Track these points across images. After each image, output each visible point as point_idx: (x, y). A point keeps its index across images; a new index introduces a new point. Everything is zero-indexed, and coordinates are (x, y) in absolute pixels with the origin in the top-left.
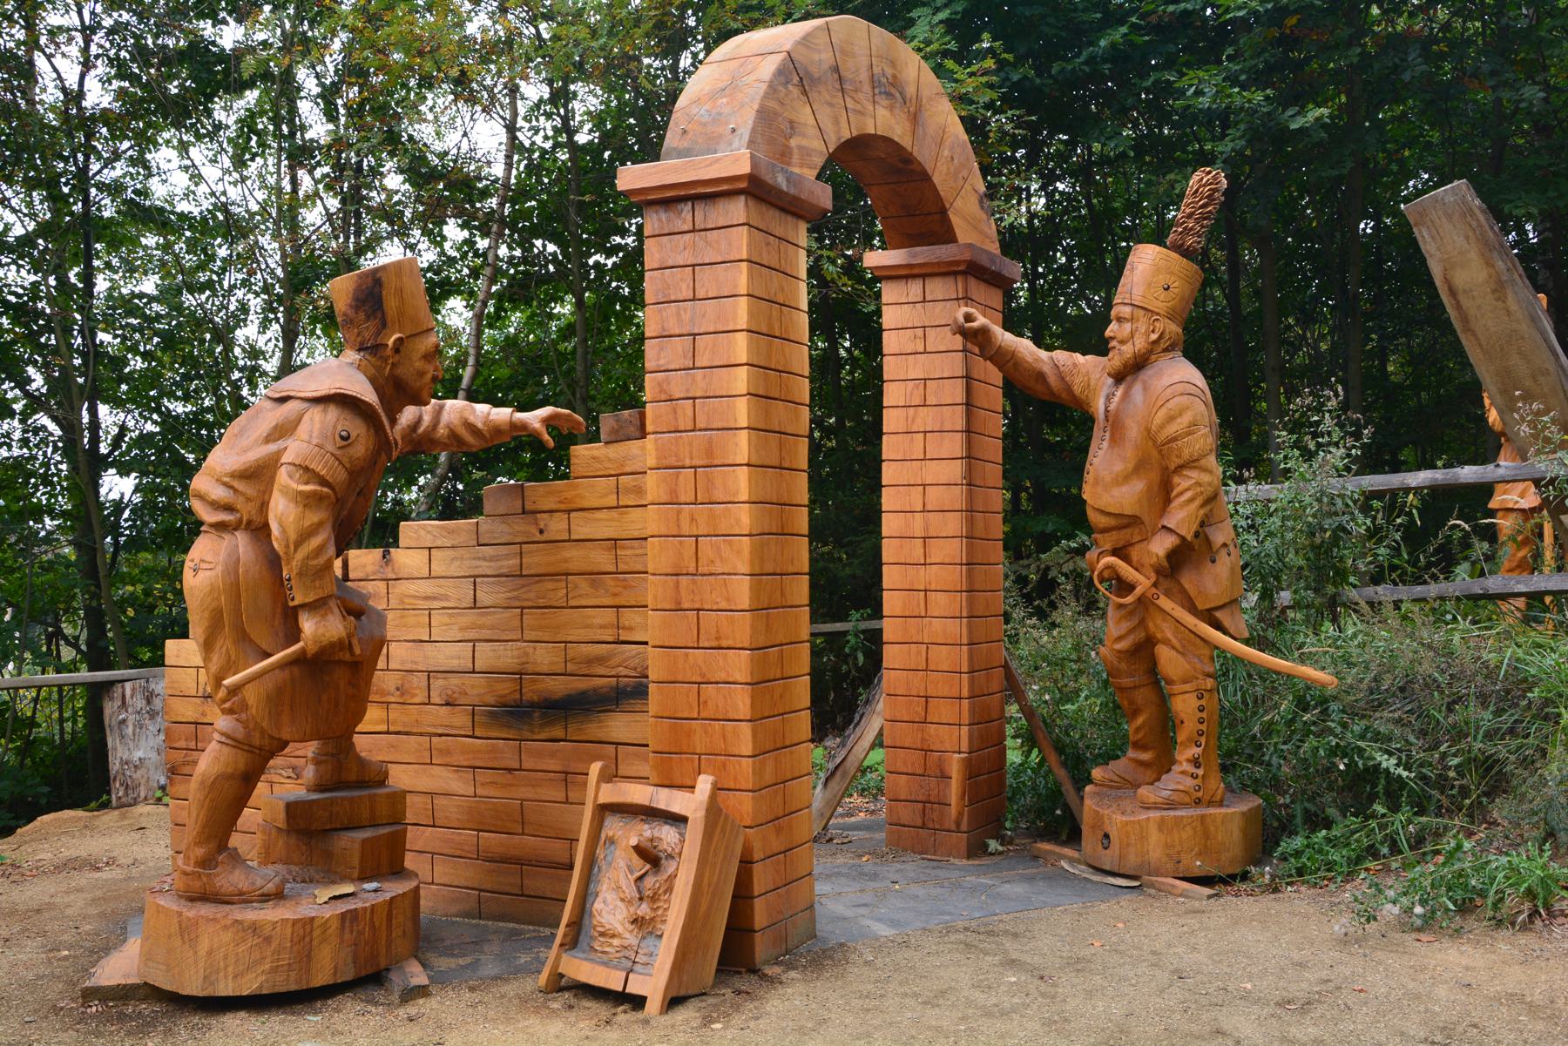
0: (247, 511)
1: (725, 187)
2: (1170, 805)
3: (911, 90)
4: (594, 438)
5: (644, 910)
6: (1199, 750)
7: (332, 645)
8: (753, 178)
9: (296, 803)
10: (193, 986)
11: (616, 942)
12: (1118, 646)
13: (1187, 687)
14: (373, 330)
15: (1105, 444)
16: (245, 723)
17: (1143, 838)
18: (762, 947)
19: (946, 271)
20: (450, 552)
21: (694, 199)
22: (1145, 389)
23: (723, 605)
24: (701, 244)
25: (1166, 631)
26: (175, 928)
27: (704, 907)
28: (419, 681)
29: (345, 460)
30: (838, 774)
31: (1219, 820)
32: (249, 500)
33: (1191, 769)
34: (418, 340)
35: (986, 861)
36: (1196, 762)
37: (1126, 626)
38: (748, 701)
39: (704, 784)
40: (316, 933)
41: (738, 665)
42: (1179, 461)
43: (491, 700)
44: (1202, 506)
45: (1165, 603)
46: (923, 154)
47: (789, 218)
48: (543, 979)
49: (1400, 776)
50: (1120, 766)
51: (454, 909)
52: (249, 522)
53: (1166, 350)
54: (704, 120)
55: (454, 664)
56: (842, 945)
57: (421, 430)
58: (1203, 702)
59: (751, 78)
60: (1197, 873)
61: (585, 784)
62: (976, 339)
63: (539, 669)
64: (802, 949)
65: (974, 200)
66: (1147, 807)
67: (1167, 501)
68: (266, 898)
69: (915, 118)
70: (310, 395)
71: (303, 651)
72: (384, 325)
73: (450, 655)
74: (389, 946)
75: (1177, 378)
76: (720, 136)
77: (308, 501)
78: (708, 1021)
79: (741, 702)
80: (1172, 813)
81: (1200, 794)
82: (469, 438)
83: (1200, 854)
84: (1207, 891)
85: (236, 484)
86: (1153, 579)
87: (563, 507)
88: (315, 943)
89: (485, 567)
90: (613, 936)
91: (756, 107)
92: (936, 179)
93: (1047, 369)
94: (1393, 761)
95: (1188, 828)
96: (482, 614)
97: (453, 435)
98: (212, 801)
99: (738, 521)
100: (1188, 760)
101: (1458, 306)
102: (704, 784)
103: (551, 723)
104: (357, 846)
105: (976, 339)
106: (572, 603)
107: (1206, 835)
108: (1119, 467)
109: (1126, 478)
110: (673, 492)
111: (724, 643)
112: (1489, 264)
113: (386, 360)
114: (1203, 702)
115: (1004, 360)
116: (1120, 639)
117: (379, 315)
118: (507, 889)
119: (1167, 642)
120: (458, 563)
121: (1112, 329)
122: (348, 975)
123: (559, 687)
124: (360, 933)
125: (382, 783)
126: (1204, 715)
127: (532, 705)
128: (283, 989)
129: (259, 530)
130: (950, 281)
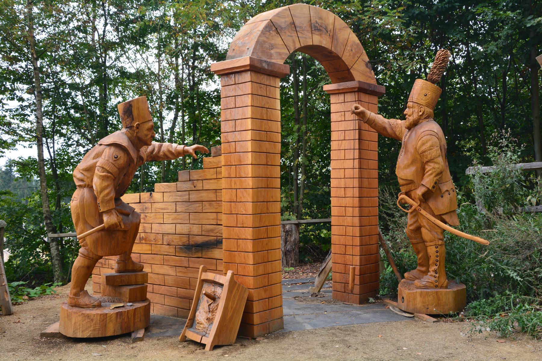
0: (87, 181)
1: (243, 69)
2: (426, 287)
3: (331, 27)
4: (209, 155)
5: (210, 315)
6: (436, 267)
7: (113, 225)
8: (250, 65)
9: (109, 276)
10: (70, 335)
11: (202, 326)
12: (411, 228)
13: (432, 244)
14: (129, 121)
15: (403, 153)
16: (87, 250)
17: (415, 299)
18: (256, 330)
19: (351, 91)
20: (169, 194)
22: (416, 133)
23: (244, 213)
24: (237, 89)
25: (424, 223)
26: (66, 315)
27: (230, 314)
28: (160, 236)
29: (116, 165)
30: (323, 272)
32: (88, 178)
33: (434, 274)
34: (145, 124)
35: (370, 305)
36: (435, 271)
37: (413, 220)
38: (252, 246)
39: (229, 273)
40: (108, 319)
41: (248, 233)
42: (427, 160)
44: (436, 176)
45: (423, 212)
46: (338, 50)
47: (271, 78)
48: (180, 338)
49: (517, 280)
50: (414, 272)
51: (171, 314)
52: (88, 185)
53: (425, 118)
54: (240, 45)
55: (170, 231)
56: (290, 331)
57: (154, 153)
58: (438, 249)
59: (257, 29)
60: (435, 313)
61: (198, 271)
62: (361, 115)
63: (194, 234)
64: (276, 333)
65: (363, 64)
67: (424, 175)
68: (94, 307)
69: (333, 37)
70: (108, 143)
71: (104, 227)
72: (133, 119)
73: (169, 228)
74: (134, 324)
75: (427, 129)
76: (244, 51)
77: (103, 178)
78: (225, 353)
79: (249, 246)
80: (425, 290)
81: (437, 284)
83: (436, 306)
84: (435, 320)
85: (84, 173)
86: (419, 203)
87: (200, 178)
88: (108, 321)
89: (179, 199)
90: (201, 324)
91: (256, 40)
92: (343, 58)
93: (387, 126)
94: (515, 274)
95: (431, 296)
96: (178, 215)
98: (78, 275)
99: (248, 184)
100: (433, 271)
103: (197, 252)
104: (128, 291)
105: (361, 115)
106: (204, 211)
107: (439, 299)
108: (406, 162)
109: (408, 166)
110: (229, 174)
111: (245, 226)
113: (134, 131)
114: (438, 249)
115: (371, 123)
116: (411, 225)
117: (131, 116)
118: (185, 308)
119: (424, 227)
120: (171, 197)
121: (407, 111)
122: (119, 333)
123: (200, 240)
125: (141, 270)
126: (438, 254)
127: (192, 246)
128: (97, 336)
129: (90, 187)
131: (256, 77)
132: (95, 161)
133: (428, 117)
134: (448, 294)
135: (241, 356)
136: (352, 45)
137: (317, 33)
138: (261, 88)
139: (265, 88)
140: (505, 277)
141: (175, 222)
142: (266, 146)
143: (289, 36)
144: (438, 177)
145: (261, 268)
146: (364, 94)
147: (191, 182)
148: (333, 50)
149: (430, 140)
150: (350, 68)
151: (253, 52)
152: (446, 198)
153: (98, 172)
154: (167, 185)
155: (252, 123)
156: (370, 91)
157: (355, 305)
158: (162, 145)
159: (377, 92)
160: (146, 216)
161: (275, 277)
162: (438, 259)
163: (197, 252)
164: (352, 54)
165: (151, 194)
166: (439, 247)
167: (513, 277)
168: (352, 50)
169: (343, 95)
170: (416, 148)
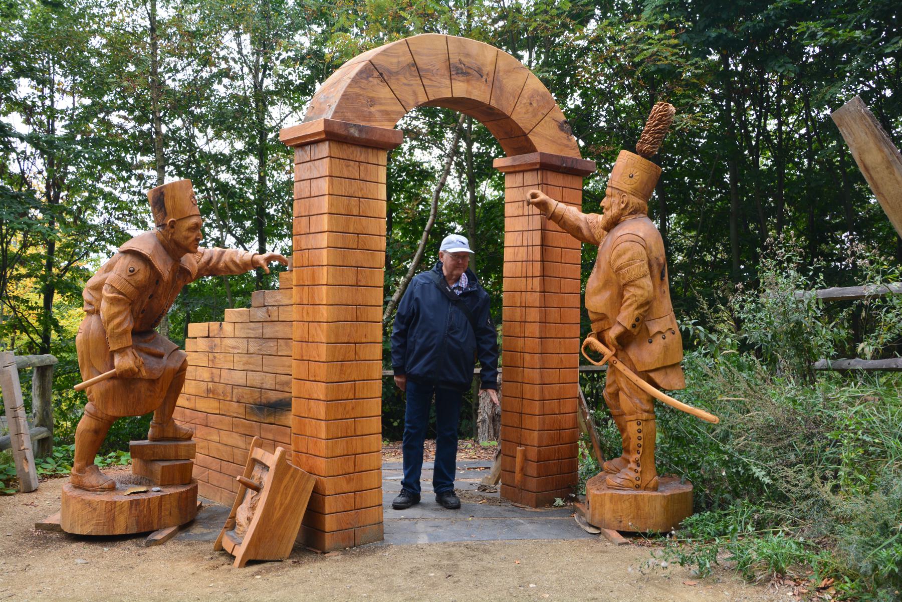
2: (621, 487)
3: (489, 68)
6: (638, 456)
7: (126, 371)
8: (326, 132)
13: (632, 417)
16: (95, 406)
17: (602, 505)
18: (328, 541)
20: (240, 325)
21: (302, 146)
23: (317, 359)
27: (277, 515)
28: (229, 388)
29: (132, 282)
31: (646, 499)
39: (279, 450)
40: (117, 509)
42: (624, 282)
43: (251, 401)
44: (637, 308)
45: (620, 366)
53: (630, 214)
58: (640, 427)
65: (554, 125)
66: (610, 487)
68: (103, 490)
69: (494, 83)
71: (115, 373)
72: (166, 214)
73: (239, 377)
74: (160, 519)
75: (627, 231)
77: (112, 301)
79: (320, 410)
81: (639, 482)
82: (233, 268)
84: (624, 540)
95: (627, 503)
97: (227, 267)
101: (872, 178)
102: (279, 450)
104: (160, 469)
105: (542, 205)
106: (279, 354)
107: (638, 508)
110: (302, 300)
112: (881, 151)
114: (640, 427)
122: (134, 531)
124: (141, 511)
126: (641, 435)
127: (265, 405)
130: (535, 173)
131: (337, 151)
132: (105, 275)
133: (635, 212)
134: (654, 502)
135: (275, 580)
136: (533, 96)
137: (461, 78)
138: (348, 166)
139: (357, 168)
140: (749, 476)
141: (246, 368)
142: (357, 257)
143: (405, 84)
144: (641, 311)
145: (341, 447)
146: (554, 174)
147: (264, 309)
148: (493, 103)
149: (629, 250)
150: (527, 132)
151: (335, 112)
152: (658, 344)
153: (106, 293)
154: (238, 312)
155: (330, 221)
156: (565, 168)
157: (528, 509)
158: (223, 252)
159: (577, 170)
160: (215, 357)
161: (366, 461)
162: (641, 442)
163: (269, 415)
164: (531, 109)
165: (221, 324)
166: (644, 423)
167: (758, 477)
168: (531, 104)
169: (521, 174)
170: (610, 262)
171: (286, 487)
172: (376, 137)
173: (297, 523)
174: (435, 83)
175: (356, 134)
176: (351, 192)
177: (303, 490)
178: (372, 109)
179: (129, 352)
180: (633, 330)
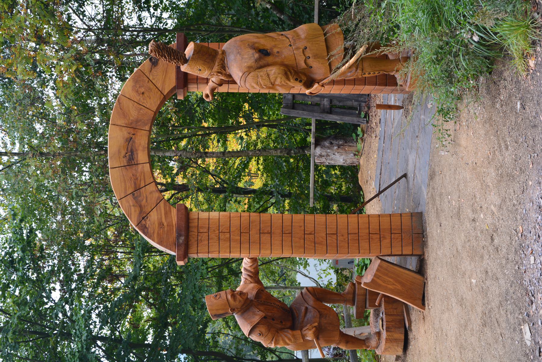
7: (315, 335)
53: (225, 70)
97: (254, 269)
136: (137, 91)
139: (202, 235)
143: (147, 201)
144: (290, 77)
168: (143, 93)
171: (384, 282)
172: (183, 224)
173: (405, 273)
174: (142, 177)
175: (183, 238)
176: (216, 238)
177: (386, 270)
178: (165, 224)
179: (304, 333)
180: (303, 82)
